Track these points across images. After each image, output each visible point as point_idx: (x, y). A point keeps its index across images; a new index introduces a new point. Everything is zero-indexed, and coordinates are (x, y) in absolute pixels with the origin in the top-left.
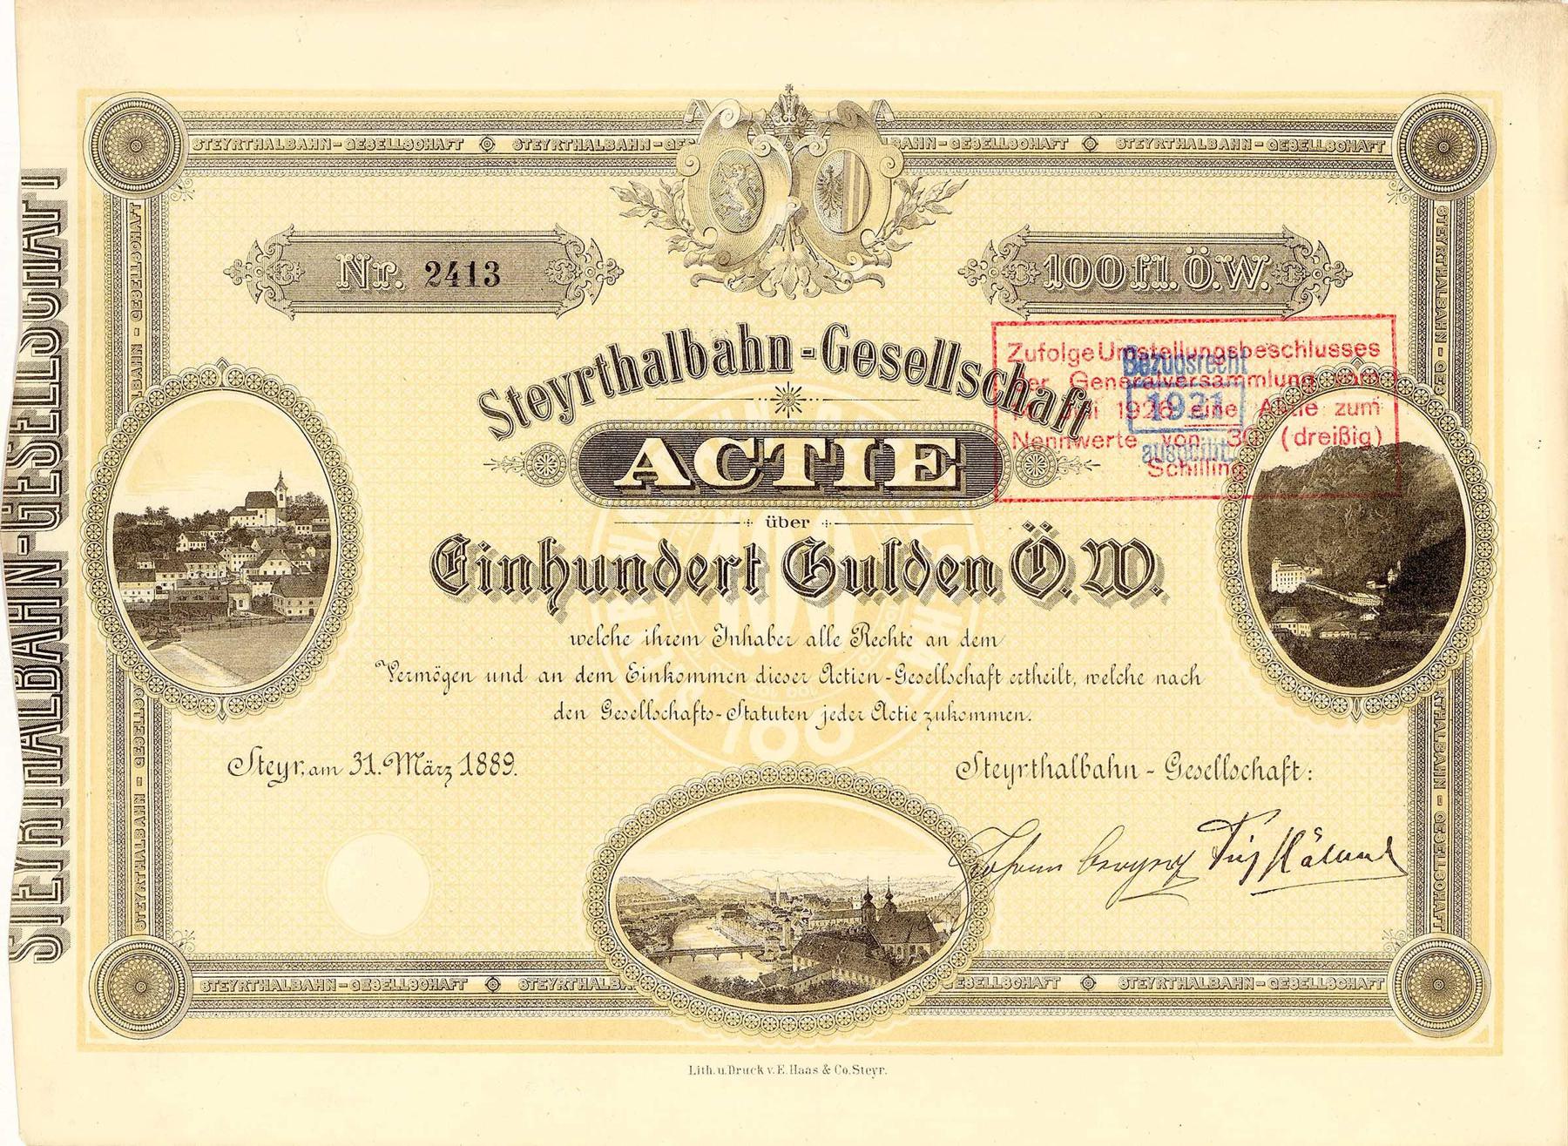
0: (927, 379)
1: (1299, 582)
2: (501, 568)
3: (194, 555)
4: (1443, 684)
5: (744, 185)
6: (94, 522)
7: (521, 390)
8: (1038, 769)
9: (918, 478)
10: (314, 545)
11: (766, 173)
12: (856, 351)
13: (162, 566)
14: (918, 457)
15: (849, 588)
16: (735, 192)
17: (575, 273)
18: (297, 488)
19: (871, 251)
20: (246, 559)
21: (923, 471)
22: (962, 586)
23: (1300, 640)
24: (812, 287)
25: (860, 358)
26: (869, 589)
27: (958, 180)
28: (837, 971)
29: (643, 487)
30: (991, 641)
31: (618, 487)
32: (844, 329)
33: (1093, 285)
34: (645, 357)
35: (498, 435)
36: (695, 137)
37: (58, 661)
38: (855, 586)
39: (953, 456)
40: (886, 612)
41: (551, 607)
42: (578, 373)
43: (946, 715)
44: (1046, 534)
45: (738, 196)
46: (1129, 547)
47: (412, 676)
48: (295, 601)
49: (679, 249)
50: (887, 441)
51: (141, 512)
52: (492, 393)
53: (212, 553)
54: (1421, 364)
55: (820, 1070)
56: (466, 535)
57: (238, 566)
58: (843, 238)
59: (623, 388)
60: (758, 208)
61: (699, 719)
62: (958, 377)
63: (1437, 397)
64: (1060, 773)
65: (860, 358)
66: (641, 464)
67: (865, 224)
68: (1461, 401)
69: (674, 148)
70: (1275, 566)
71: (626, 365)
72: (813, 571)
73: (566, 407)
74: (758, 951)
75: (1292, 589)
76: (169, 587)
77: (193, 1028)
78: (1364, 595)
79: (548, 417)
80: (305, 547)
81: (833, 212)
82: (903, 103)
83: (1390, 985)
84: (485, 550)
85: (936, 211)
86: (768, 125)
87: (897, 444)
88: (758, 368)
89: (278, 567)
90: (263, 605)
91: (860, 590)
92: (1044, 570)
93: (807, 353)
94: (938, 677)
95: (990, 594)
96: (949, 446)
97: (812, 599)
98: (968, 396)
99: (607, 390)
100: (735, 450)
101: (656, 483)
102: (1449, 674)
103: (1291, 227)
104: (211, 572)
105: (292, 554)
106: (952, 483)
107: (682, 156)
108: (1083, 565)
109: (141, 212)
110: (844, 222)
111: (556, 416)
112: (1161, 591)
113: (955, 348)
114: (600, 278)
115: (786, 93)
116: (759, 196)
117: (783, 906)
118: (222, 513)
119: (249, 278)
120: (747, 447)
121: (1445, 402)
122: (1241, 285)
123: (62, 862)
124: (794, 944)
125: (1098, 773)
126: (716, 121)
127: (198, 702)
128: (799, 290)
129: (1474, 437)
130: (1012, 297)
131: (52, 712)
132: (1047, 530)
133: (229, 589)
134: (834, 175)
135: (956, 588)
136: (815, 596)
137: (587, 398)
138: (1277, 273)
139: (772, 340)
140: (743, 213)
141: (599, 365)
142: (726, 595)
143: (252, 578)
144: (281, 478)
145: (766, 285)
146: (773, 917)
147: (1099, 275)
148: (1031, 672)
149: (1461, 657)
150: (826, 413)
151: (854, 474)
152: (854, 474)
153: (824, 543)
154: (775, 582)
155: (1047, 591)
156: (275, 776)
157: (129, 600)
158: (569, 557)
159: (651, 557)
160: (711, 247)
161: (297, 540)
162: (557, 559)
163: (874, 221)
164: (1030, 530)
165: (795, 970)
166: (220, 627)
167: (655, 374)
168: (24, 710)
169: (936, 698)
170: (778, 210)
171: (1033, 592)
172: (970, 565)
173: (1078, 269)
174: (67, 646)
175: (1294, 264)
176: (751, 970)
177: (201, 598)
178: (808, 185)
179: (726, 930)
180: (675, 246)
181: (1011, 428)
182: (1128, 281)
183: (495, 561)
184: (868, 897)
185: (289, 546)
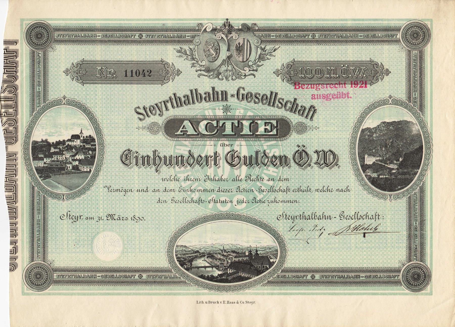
0: (268, 103)
1: (374, 161)
2: (141, 159)
3: (55, 153)
4: (417, 191)
5: (214, 48)
6: (26, 143)
7: (147, 106)
8: (301, 217)
9: (265, 132)
10: (91, 150)
11: (220, 45)
12: (247, 95)
13: (46, 156)
14: (265, 126)
15: (245, 164)
16: (211, 50)
17: (167, 72)
18: (86, 133)
19: (251, 67)
20: (71, 154)
21: (267, 130)
22: (278, 163)
23: (374, 178)
24: (234, 77)
25: (248, 97)
26: (251, 164)
27: (277, 47)
28: (241, 273)
29: (184, 135)
30: (287, 179)
31: (176, 135)
32: (243, 88)
33: (314, 76)
34: (184, 97)
35: (140, 119)
36: (199, 34)
37: (15, 183)
38: (247, 163)
39: (275, 125)
40: (256, 171)
41: (156, 170)
42: (164, 102)
43: (274, 201)
44: (304, 148)
45: (212, 51)
46: (328, 152)
47: (115, 190)
48: (85, 167)
49: (195, 67)
50: (256, 121)
51: (40, 140)
52: (139, 108)
53: (60, 153)
54: (409, 98)
55: (236, 302)
56: (131, 149)
57: (68, 156)
58: (243, 63)
59: (177, 106)
60: (218, 55)
61: (200, 203)
62: (277, 102)
63: (415, 107)
64: (308, 218)
65: (248, 97)
66: (183, 128)
67: (250, 59)
68: (422, 107)
69: (193, 37)
70: (366, 156)
71: (178, 99)
72: (234, 159)
73: (160, 111)
74: (217, 267)
75: (371, 163)
76: (48, 162)
77: (52, 289)
78: (392, 165)
79: (155, 115)
80: (88, 151)
81: (240, 56)
82: (261, 24)
83: (401, 277)
84: (136, 153)
85: (271, 55)
86: (220, 30)
87: (259, 122)
88: (218, 100)
89: (80, 157)
90: (76, 168)
91: (248, 165)
92: (303, 159)
93: (232, 96)
94: (272, 190)
95: (287, 166)
96: (274, 122)
97: (234, 167)
98: (279, 108)
99: (173, 107)
100: (210, 124)
101: (188, 134)
102: (418, 188)
103: (373, 59)
104: (60, 158)
105: (85, 153)
106: (276, 133)
107: (197, 40)
108: (314, 157)
109: (40, 55)
110: (243, 58)
111: (157, 114)
112: (338, 164)
113: (276, 94)
114: (175, 74)
115: (226, 21)
116: (218, 51)
117: (225, 254)
118: (64, 141)
119: (70, 74)
120: (215, 123)
121: (417, 108)
122: (358, 76)
123: (15, 242)
124: (228, 265)
125: (319, 218)
126: (205, 29)
127: (57, 196)
128: (230, 78)
129: (428, 119)
130: (290, 79)
131: (13, 198)
132: (304, 147)
133: (66, 163)
134: (240, 45)
135: (277, 164)
136: (235, 167)
137: (167, 109)
138: (368, 72)
139: (222, 92)
140: (213, 56)
141: (170, 99)
142: (208, 166)
143: (72, 160)
144: (81, 131)
145: (220, 77)
146: (222, 257)
147: (315, 74)
148: (299, 188)
149: (422, 183)
150: (239, 113)
151: (246, 131)
152: (246, 131)
153: (237, 151)
154: (222, 162)
155: (304, 165)
156: (74, 220)
157: (36, 166)
158: (161, 155)
159: (186, 154)
160: (204, 66)
161: (87, 148)
162: (158, 156)
163: (252, 58)
164: (299, 147)
165: (229, 273)
166: (63, 174)
167: (187, 101)
168: (7, 197)
169: (272, 196)
170: (224, 54)
171: (300, 165)
172: (281, 157)
173: (318, 72)
174: (17, 179)
175: (373, 69)
176: (216, 273)
177: (57, 166)
178: (233, 48)
179: (207, 260)
180: (193, 65)
181: (294, 118)
182: (324, 74)
183: (140, 156)
184: (250, 251)
185: (84, 151)
